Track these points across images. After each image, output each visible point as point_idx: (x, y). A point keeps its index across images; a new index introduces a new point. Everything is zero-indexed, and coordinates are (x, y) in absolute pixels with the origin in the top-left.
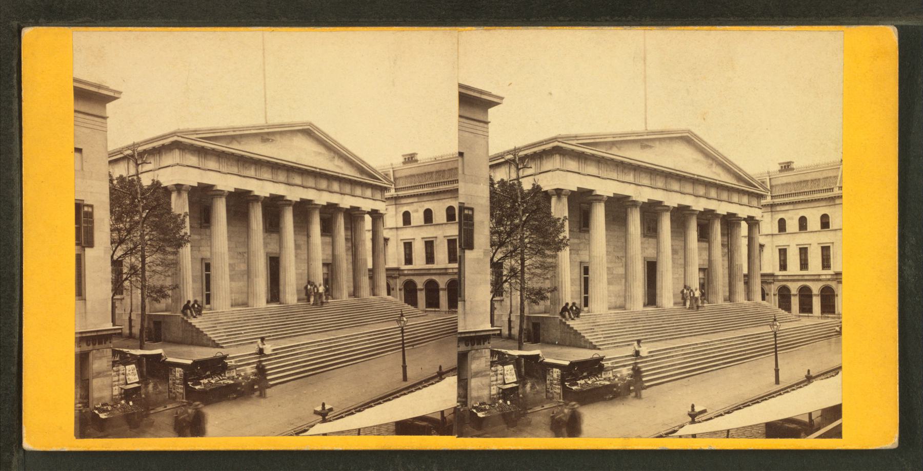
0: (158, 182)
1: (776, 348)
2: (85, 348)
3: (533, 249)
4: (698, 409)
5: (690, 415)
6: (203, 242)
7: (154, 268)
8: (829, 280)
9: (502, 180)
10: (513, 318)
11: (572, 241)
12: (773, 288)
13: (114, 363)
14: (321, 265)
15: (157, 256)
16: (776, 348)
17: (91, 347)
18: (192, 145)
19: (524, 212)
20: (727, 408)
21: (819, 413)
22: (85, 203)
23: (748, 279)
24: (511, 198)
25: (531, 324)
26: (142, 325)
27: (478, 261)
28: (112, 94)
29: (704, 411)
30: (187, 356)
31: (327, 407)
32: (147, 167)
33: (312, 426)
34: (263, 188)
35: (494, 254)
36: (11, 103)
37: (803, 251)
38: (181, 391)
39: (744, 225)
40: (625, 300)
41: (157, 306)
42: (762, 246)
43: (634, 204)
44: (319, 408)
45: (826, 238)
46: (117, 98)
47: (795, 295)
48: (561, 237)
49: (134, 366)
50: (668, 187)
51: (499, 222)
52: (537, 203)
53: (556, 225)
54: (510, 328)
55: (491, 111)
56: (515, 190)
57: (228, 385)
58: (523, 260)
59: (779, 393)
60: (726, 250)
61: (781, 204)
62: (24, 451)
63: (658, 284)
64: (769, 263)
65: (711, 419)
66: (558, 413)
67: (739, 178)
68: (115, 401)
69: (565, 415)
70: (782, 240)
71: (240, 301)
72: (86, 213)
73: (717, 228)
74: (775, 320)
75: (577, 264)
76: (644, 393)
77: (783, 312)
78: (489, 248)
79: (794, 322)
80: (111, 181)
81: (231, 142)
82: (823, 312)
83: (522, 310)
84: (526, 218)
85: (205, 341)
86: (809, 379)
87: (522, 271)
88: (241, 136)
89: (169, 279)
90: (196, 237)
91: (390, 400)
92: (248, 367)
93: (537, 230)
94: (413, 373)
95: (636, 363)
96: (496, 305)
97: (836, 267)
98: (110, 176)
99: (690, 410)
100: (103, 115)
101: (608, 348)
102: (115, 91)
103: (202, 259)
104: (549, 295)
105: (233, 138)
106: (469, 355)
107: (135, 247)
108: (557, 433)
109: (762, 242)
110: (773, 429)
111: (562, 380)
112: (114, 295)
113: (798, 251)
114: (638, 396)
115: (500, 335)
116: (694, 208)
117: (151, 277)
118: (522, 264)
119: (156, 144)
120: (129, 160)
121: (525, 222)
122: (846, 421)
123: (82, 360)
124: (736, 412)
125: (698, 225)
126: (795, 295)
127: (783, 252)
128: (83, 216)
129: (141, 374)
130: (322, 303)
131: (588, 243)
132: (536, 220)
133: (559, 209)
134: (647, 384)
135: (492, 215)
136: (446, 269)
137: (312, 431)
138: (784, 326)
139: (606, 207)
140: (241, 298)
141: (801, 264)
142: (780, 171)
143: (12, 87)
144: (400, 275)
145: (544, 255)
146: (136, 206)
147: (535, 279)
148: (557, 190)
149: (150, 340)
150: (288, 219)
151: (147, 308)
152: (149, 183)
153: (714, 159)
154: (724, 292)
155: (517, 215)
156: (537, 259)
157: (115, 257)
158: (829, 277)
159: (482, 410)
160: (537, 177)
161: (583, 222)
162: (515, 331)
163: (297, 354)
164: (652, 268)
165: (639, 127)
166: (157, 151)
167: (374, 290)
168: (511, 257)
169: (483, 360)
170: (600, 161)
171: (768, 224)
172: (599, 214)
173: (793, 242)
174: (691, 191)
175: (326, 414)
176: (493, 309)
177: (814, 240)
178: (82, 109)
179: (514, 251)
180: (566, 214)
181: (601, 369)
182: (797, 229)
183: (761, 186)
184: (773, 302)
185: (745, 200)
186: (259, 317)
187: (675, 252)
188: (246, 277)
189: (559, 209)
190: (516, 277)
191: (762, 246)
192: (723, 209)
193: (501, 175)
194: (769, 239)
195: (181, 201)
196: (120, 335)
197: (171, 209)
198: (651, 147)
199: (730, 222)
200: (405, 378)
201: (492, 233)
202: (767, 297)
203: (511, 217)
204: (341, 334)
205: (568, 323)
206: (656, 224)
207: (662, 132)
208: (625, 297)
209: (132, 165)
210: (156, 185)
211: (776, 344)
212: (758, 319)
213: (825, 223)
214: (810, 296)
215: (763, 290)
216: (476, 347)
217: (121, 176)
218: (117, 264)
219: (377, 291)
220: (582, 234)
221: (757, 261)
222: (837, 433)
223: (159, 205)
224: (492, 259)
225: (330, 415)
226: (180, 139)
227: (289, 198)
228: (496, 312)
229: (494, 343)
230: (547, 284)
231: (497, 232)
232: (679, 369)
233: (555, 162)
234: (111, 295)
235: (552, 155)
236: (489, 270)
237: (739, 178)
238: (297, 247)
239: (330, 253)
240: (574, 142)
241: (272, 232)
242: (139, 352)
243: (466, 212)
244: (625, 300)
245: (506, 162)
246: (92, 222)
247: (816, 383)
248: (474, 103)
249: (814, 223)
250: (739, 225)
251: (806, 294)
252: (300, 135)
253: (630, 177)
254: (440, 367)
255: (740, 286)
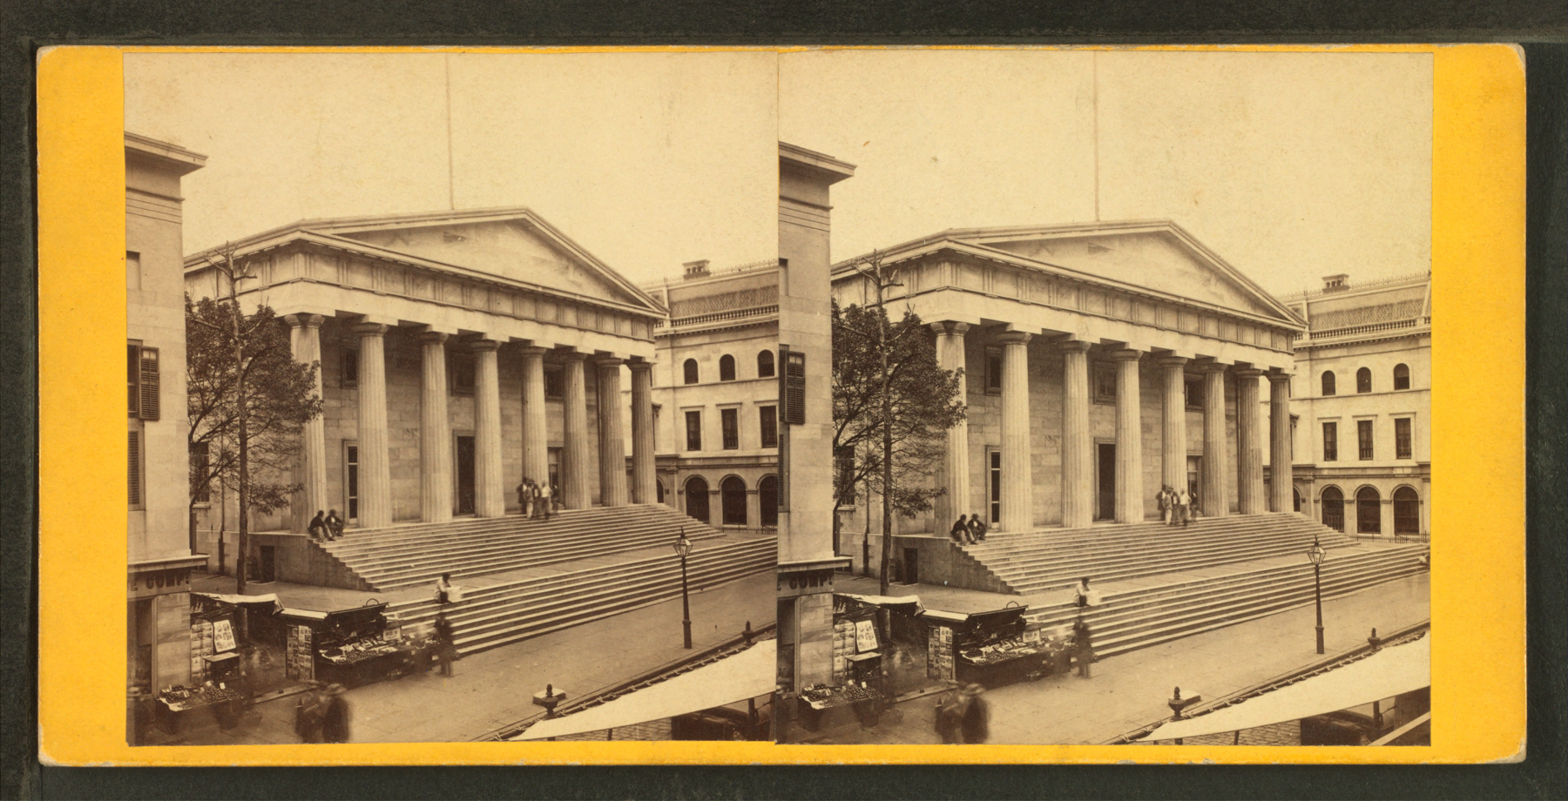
0: (268, 309)
1: (1318, 591)
2: (144, 591)
3: (261, 419)
4: (1185, 695)
5: (1172, 706)
6: (345, 412)
7: (262, 456)
8: (1408, 476)
9: (853, 306)
10: (871, 542)
11: (972, 409)
12: (1314, 491)
13: (194, 618)
14: (545, 451)
15: (267, 436)
16: (1318, 591)
17: (154, 591)
18: (326, 247)
19: (890, 361)
20: (1235, 693)
21: (1392, 702)
22: (145, 344)
23: (1270, 475)
24: (222, 330)
25: (901, 552)
26: (241, 554)
27: (812, 443)
28: (189, 160)
29: (1196, 700)
30: (318, 605)
31: (556, 692)
32: (250, 284)
33: (531, 725)
34: (447, 319)
35: (839, 433)
36: (19, 175)
37: (1365, 428)
38: (308, 665)
39: (1264, 383)
40: (1062, 511)
41: (267, 520)
42: (1294, 419)
43: (1078, 346)
44: (542, 695)
45: (1403, 404)
46: (195, 167)
47: (1350, 502)
48: (953, 404)
49: (227, 622)
50: (1136, 319)
51: (848, 378)
52: (913, 346)
53: (944, 382)
54: (866, 558)
55: (833, 188)
56: (875, 323)
57: (388, 655)
58: (888, 442)
59: (1323, 668)
60: (1233, 426)
61: (1327, 347)
62: (42, 767)
63: (1119, 483)
64: (1306, 448)
65: (1208, 712)
66: (948, 703)
67: (1256, 303)
68: (195, 682)
69: (960, 706)
70: (1329, 409)
71: (408, 512)
72: (147, 363)
73: (1218, 387)
74: (1317, 544)
75: (981, 449)
76: (1094, 668)
77: (1330, 531)
78: (830, 421)
79: (1349, 548)
80: (189, 307)
81: (392, 242)
82: (1398, 530)
83: (887, 527)
84: (893, 371)
85: (348, 581)
86: (1375, 644)
87: (887, 460)
88: (410, 231)
89: (286, 474)
90: (334, 403)
91: (662, 680)
92: (421, 625)
93: (912, 391)
94: (702, 635)
95: (1081, 618)
96: (843, 519)
97: (1419, 453)
98: (187, 299)
99: (1172, 697)
100: (174, 195)
101: (1033, 592)
102: (195, 156)
103: (343, 441)
104: (932, 501)
105: (395, 235)
106: (797, 603)
107: (229, 421)
108: (947, 737)
109: (1295, 412)
110: (1314, 730)
111: (955, 647)
112: (193, 502)
113: (1355, 428)
114: (1084, 674)
115: (849, 570)
116: (1179, 354)
117: (256, 471)
118: (888, 449)
119: (265, 245)
120: (219, 271)
121: (892, 377)
122: (1437, 715)
123: (140, 613)
124: (1250, 701)
125: (1186, 383)
126: (1350, 502)
127: (1330, 429)
128: (141, 367)
129: (239, 636)
130: (548, 515)
131: (1000, 412)
132: (910, 374)
133: (950, 356)
134: (1099, 653)
135: (835, 366)
136: (758, 457)
137: (529, 733)
138: (1332, 555)
139: (1029, 351)
140: (409, 507)
141: (1361, 450)
142: (1325, 291)
143: (21, 147)
144: (679, 468)
145: (924, 434)
146: (879, 357)
147: (909, 475)
148: (946, 323)
149: (255, 577)
150: (490, 373)
151: (251, 523)
152: (254, 311)
153: (1213, 271)
154: (1230, 496)
155: (879, 365)
156: (913, 440)
157: (196, 438)
158: (1408, 471)
159: (818, 697)
160: (912, 301)
161: (990, 378)
162: (876, 563)
163: (505, 602)
164: (1107, 456)
165: (1085, 216)
166: (267, 258)
167: (635, 494)
168: (869, 436)
169: (821, 613)
170: (1019, 274)
171: (1305, 381)
172: (1018, 364)
173: (1346, 411)
174: (1173, 325)
175: (554, 705)
176: (837, 525)
177: (1383, 408)
178: (794, 195)
179: (873, 427)
180: (962, 364)
181: (1022, 627)
182: (1353, 389)
183: (1293, 316)
184: (1313, 514)
185: (1266, 339)
186: (440, 539)
187: (1146, 428)
188: (417, 470)
189: (950, 356)
190: (877, 471)
191: (1294, 419)
192: (1228, 355)
193: (851, 297)
194: (1306, 406)
195: (308, 341)
196: (204, 570)
197: (290, 355)
198: (1105, 250)
199: (1240, 377)
200: (688, 644)
201: (836, 397)
202: (1302, 506)
203: (868, 368)
204: (579, 568)
205: (964, 549)
206: (1115, 381)
207: (1124, 225)
208: (1062, 505)
209: (224, 281)
210: (265, 315)
211: (1318, 585)
212: (1288, 542)
213: (1402, 379)
214: (1376, 504)
215: (1296, 493)
216: (808, 589)
217: (206, 300)
218: (198, 450)
219: (640, 495)
220: (989, 399)
221: (1286, 444)
222: (1421, 736)
223: (269, 348)
224: (835, 441)
225: (561, 705)
226: (306, 237)
227: (490, 337)
228: (843, 531)
229: (839, 584)
230: (930, 484)
231: (844, 395)
232: (1153, 627)
233: (944, 275)
234: (189, 502)
235: (939, 263)
236: (831, 459)
237: (1256, 303)
238: (505, 420)
239: (561, 430)
240: (329, 233)
241: (462, 395)
242: (236, 599)
243: (792, 360)
244: (1062, 511)
245: (860, 276)
246: (157, 378)
247: (1386, 652)
248: (805, 176)
249: (1383, 379)
250: (1256, 382)
251: (1369, 500)
252: (509, 229)
253: (1071, 302)
254: (748, 624)
255: (1258, 487)
